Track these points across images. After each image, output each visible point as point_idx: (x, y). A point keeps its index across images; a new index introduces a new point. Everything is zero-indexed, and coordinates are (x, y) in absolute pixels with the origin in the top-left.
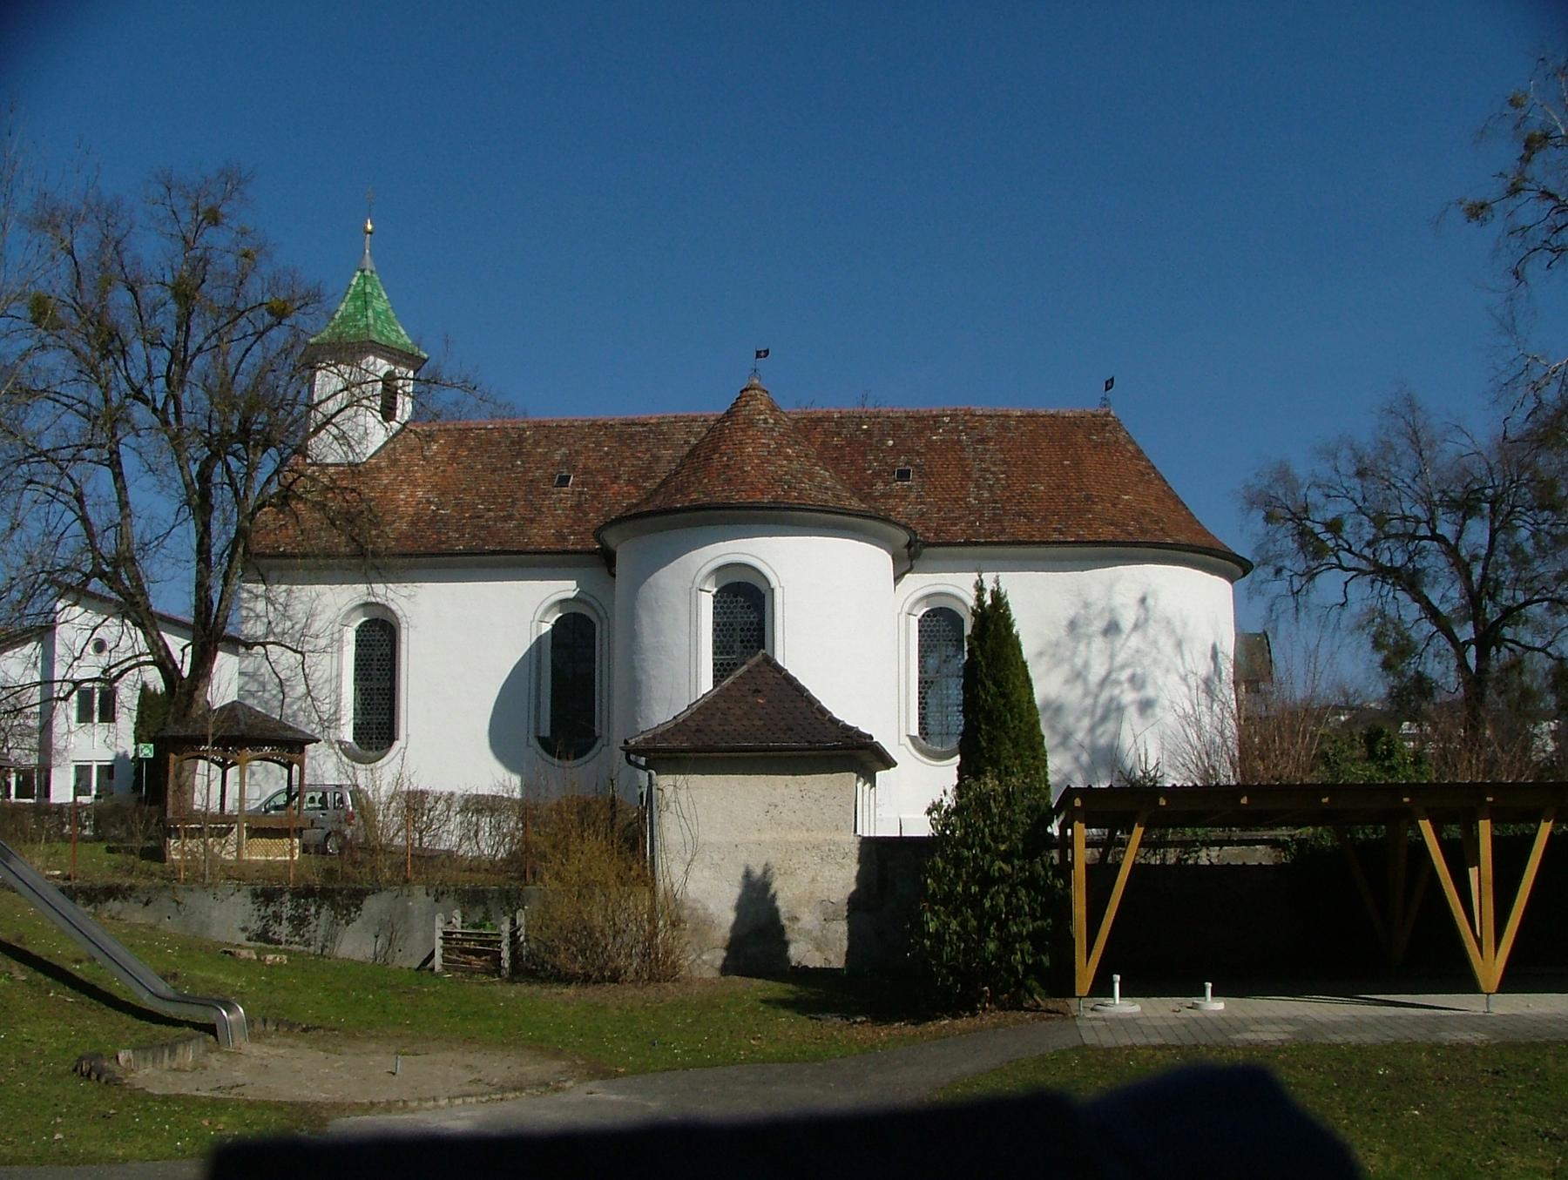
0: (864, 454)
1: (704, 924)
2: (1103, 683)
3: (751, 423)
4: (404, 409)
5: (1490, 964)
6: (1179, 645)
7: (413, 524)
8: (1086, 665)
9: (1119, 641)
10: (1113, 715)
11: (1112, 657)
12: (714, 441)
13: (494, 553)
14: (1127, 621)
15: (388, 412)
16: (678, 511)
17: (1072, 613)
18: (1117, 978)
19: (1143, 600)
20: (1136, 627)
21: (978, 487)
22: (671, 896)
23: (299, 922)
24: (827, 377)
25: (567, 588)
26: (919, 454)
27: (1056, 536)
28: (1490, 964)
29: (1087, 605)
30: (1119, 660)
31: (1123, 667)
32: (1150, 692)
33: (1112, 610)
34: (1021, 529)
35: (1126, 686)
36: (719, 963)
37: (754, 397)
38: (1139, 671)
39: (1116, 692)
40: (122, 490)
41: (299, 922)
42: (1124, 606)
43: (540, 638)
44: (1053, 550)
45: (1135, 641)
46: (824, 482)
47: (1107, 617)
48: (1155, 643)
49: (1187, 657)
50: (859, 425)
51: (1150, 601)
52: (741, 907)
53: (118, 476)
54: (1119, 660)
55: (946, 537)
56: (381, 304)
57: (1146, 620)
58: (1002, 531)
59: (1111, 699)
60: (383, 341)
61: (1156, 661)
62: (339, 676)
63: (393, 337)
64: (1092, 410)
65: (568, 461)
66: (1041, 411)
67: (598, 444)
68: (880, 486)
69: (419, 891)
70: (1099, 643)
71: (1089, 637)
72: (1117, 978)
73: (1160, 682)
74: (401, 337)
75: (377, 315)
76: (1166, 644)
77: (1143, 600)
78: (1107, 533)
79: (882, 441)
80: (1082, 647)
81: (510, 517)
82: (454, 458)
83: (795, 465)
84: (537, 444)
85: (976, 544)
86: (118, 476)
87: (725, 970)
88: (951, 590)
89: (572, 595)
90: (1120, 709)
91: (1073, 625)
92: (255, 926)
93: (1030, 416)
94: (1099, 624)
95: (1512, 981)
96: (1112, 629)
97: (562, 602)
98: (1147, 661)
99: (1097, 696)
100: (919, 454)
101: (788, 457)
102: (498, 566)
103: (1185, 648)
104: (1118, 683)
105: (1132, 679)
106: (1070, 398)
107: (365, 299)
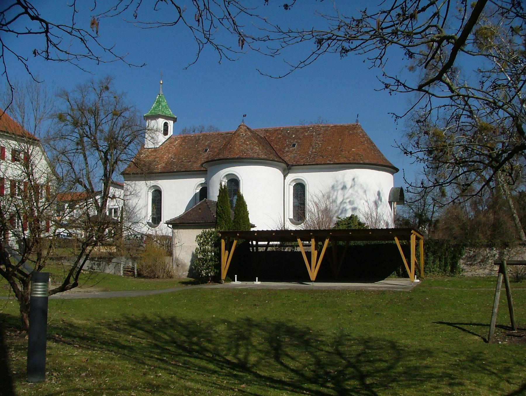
0: (285, 140)
1: (184, 265)
2: (341, 203)
3: (239, 135)
4: (171, 132)
5: (313, 274)
6: (365, 192)
7: (166, 164)
8: (336, 198)
9: (346, 191)
10: (344, 212)
11: (344, 196)
12: (229, 139)
13: (183, 171)
14: (348, 185)
15: (166, 132)
16: (215, 160)
17: (333, 184)
18: (236, 276)
19: (354, 179)
20: (351, 187)
21: (313, 148)
22: (177, 259)
23: (99, 265)
24: (263, 122)
25: (202, 180)
26: (300, 139)
27: (328, 162)
28: (313, 274)
29: (337, 181)
30: (346, 196)
31: (347, 198)
32: (355, 205)
33: (344, 182)
34: (319, 160)
35: (348, 204)
36: (187, 275)
37: (241, 128)
38: (352, 199)
39: (345, 205)
40: (86, 160)
41: (99, 265)
42: (348, 181)
43: (196, 194)
44: (328, 166)
45: (351, 191)
46: (258, 150)
47: (343, 184)
48: (357, 192)
49: (368, 196)
50: (287, 131)
51: (356, 180)
52: (192, 261)
53: (85, 156)
54: (346, 196)
55: (298, 163)
56: (164, 104)
57: (354, 185)
58: (314, 161)
59: (343, 208)
60: (164, 114)
61: (357, 196)
62: (147, 204)
63: (167, 112)
64: (353, 123)
65: (209, 146)
66: (338, 125)
67: (218, 140)
68: (287, 149)
69: (123, 258)
70: (340, 192)
71: (338, 190)
72: (236, 276)
73: (358, 203)
74: (169, 112)
75: (162, 107)
76: (360, 192)
77: (354, 179)
78: (342, 161)
79: (292, 136)
80: (336, 193)
81: (190, 161)
82: (181, 145)
83: (249, 146)
84: (202, 140)
85: (306, 165)
86: (85, 156)
87: (188, 276)
88: (301, 178)
89: (203, 182)
90: (346, 210)
91: (333, 187)
92: (90, 266)
93: (335, 126)
94: (340, 187)
95: (319, 279)
96: (344, 188)
97: (201, 184)
98: (354, 197)
99: (339, 207)
100: (300, 139)
101: (247, 145)
102: (186, 175)
103: (367, 192)
104: (345, 203)
105: (350, 202)
106: (347, 121)
107: (159, 102)
